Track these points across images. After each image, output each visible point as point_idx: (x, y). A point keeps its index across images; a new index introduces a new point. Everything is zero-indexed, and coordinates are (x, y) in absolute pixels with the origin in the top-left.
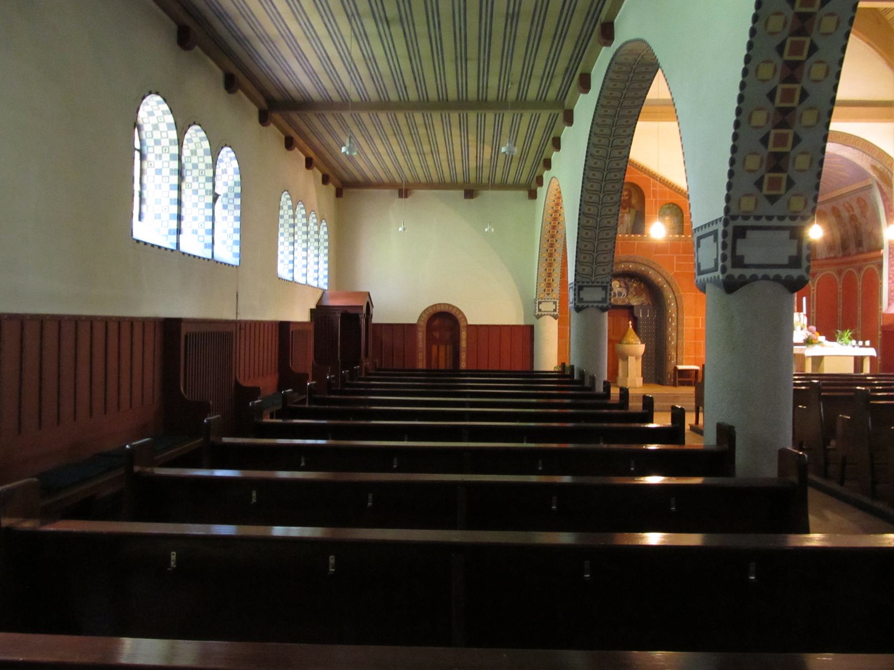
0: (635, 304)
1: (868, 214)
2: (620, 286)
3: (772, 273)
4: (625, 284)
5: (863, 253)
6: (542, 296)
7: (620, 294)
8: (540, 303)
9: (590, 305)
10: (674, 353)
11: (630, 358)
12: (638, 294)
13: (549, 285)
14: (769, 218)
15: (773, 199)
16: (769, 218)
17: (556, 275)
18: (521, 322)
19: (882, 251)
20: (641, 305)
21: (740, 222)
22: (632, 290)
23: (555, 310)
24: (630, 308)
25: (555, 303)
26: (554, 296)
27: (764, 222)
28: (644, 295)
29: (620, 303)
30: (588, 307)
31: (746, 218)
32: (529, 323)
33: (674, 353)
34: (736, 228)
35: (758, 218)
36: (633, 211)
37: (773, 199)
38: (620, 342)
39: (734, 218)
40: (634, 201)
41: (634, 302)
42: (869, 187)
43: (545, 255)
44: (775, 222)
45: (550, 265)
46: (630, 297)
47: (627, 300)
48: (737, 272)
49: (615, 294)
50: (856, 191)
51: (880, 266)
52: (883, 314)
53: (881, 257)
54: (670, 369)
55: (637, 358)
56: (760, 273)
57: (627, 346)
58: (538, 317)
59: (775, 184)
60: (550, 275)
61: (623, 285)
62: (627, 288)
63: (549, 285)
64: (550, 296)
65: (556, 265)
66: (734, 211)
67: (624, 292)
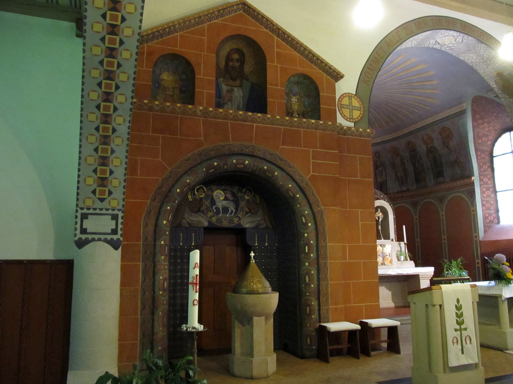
0: (247, 226)
1: (452, 144)
2: (226, 199)
3: (103, 237)
4: (233, 195)
5: (444, 182)
6: (89, 202)
7: (225, 210)
8: (84, 216)
9: (96, 237)
10: (314, 303)
11: (255, 319)
12: (251, 212)
13: (103, 182)
14: (101, 209)
15: (102, 200)
16: (101, 209)
17: (116, 162)
18: (48, 255)
19: (473, 178)
20: (256, 228)
21: (85, 211)
22: (243, 204)
23: (114, 232)
24: (239, 233)
25: (115, 217)
26: (114, 204)
27: (98, 211)
28: (260, 212)
29: (225, 224)
30: (93, 240)
31: (88, 209)
32: (63, 256)
33: (314, 303)
34: (82, 214)
35: (95, 209)
36: (247, 85)
37: (102, 200)
38: (236, 290)
39: (82, 209)
40: (248, 68)
41: (247, 223)
42: (463, 113)
43: (94, 117)
44: (104, 212)
45: (105, 140)
46: (240, 215)
47: (236, 220)
48: (84, 237)
49: (217, 209)
50: (442, 120)
51: (472, 194)
52: (480, 242)
53: (473, 184)
54: (310, 327)
55: (267, 319)
56: (96, 237)
57: (250, 299)
58: (80, 244)
59: (102, 193)
60: (104, 161)
61: (229, 196)
62: (236, 202)
63: (103, 182)
64: (105, 204)
65: (118, 141)
66: (81, 205)
67: (232, 208)
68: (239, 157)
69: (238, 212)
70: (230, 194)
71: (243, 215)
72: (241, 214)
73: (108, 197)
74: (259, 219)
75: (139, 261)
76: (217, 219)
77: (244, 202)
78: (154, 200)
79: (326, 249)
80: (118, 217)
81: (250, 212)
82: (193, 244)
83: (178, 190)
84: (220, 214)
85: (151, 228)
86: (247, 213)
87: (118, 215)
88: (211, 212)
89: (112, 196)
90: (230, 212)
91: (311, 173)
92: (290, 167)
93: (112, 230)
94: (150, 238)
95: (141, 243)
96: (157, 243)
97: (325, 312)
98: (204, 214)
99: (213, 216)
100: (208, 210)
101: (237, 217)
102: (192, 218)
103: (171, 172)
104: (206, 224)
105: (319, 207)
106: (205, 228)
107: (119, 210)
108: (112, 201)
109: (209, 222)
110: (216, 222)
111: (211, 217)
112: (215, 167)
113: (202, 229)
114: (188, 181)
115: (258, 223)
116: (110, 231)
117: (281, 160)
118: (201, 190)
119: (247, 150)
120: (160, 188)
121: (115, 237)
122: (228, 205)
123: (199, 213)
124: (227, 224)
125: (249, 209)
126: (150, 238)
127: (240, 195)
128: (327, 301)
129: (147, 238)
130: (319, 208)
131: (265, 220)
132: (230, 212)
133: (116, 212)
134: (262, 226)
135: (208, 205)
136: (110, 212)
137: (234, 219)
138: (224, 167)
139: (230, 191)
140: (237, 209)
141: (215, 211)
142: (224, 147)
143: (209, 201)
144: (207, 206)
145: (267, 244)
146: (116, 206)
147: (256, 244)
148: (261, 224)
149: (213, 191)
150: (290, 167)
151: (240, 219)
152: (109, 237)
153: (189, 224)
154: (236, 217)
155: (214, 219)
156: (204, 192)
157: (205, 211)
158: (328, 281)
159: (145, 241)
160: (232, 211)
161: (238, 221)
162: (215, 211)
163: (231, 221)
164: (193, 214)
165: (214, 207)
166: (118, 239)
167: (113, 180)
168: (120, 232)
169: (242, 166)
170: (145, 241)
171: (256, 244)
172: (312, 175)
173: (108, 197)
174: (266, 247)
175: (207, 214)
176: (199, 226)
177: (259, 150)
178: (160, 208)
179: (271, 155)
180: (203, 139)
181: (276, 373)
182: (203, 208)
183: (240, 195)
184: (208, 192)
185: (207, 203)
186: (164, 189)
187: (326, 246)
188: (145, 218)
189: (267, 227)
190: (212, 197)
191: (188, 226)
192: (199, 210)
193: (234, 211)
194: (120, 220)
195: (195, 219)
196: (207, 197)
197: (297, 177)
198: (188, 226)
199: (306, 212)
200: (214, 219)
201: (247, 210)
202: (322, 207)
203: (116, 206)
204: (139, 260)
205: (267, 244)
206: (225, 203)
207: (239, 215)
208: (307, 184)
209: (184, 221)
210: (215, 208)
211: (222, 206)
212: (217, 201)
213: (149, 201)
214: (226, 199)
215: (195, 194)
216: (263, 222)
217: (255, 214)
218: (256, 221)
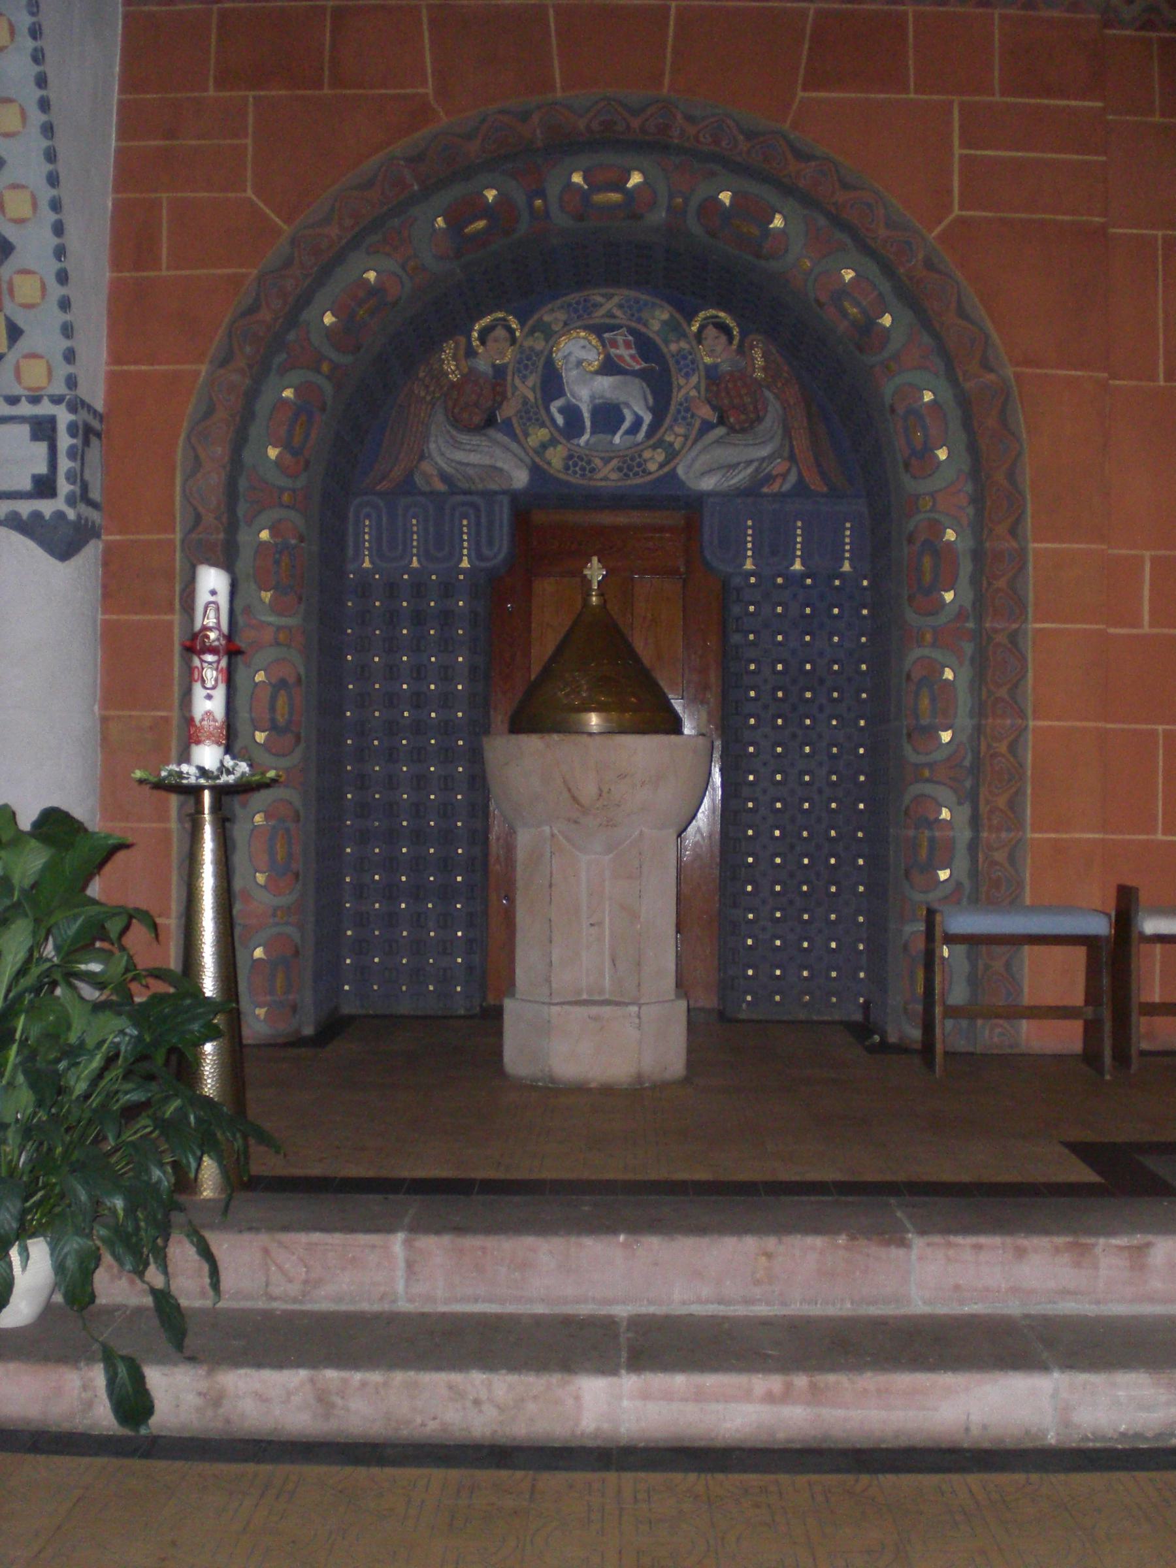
0: (708, 484)
7: (608, 416)
22: (687, 387)
23: (44, 487)
25: (43, 430)
26: (35, 374)
46: (674, 436)
47: (654, 460)
61: (625, 354)
68: (753, 188)
69: (668, 421)
70: (627, 345)
71: (686, 437)
72: (680, 430)
73: (10, 348)
74: (764, 452)
75: (171, 610)
76: (571, 457)
77: (694, 380)
78: (225, 361)
79: (1022, 567)
80: (54, 429)
81: (722, 421)
82: (465, 564)
83: (328, 319)
84: (581, 434)
85: (213, 479)
86: (707, 427)
87: (52, 420)
88: (543, 425)
89: (23, 345)
90: (626, 425)
91: (956, 212)
92: (845, 186)
93: (38, 480)
94: (209, 519)
95: (178, 537)
96: (243, 537)
97: (1000, 856)
98: (514, 436)
99: (553, 442)
100: (531, 415)
101: (660, 444)
102: (459, 456)
103: (294, 242)
104: (520, 478)
105: (992, 370)
106: (515, 497)
107: (57, 400)
108: (24, 364)
109: (536, 471)
110: (567, 468)
111: (544, 446)
112: (486, 211)
113: (505, 500)
114: (371, 276)
115: (757, 470)
116: (27, 485)
117: (801, 155)
118: (500, 332)
119: (636, 123)
120: (252, 310)
121: (47, 507)
122: (620, 396)
123: (492, 432)
124: (614, 476)
125: (714, 408)
126: (209, 519)
127: (673, 347)
128: (1014, 805)
129: (198, 518)
130: (992, 377)
131: (792, 458)
132: (626, 425)
133: (45, 408)
134: (775, 488)
135: (531, 396)
136: (25, 409)
137: (647, 454)
138: (531, 205)
139: (632, 331)
140: (659, 412)
141: (560, 420)
142: (525, 116)
143: (533, 379)
144: (525, 402)
145: (798, 566)
146: (43, 382)
147: (749, 565)
148: (769, 479)
149: (549, 335)
150: (845, 186)
151: (672, 454)
152: (25, 508)
153: (445, 477)
154: (654, 447)
155: (556, 458)
156: (513, 341)
157: (514, 421)
158: (1022, 714)
159: (191, 531)
160: (638, 422)
161: (661, 466)
162: (560, 420)
163: (631, 463)
164: (464, 438)
165: (554, 407)
166: (60, 515)
167: (18, 280)
168: (64, 487)
169: (615, 197)
170: (191, 531)
171: (749, 565)
172: (961, 221)
173: (10, 348)
174: (794, 580)
175: (526, 435)
176: (493, 487)
177: (689, 119)
178: (252, 395)
179: (750, 135)
180: (429, 90)
181: (686, 1080)
182: (509, 410)
183: (673, 347)
184: (528, 343)
185: (525, 388)
186: (265, 315)
187: (1022, 553)
188: (188, 438)
189: (801, 489)
190: (550, 363)
191: (441, 487)
192: (490, 422)
193: (647, 418)
194: (64, 441)
195: (474, 458)
196: (525, 361)
197: (883, 232)
198: (441, 487)
199: (928, 397)
200: (556, 458)
201: (706, 412)
202: (1010, 371)
203: (43, 382)
204: (172, 604)
205: (798, 566)
206: (605, 384)
207: (669, 438)
208: (929, 264)
209: (425, 466)
210: (561, 411)
211: (593, 398)
212: (570, 376)
213: (204, 368)
214: (610, 367)
215: (471, 353)
216: (779, 466)
217: (743, 431)
218: (749, 463)
